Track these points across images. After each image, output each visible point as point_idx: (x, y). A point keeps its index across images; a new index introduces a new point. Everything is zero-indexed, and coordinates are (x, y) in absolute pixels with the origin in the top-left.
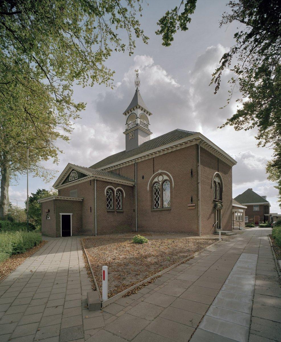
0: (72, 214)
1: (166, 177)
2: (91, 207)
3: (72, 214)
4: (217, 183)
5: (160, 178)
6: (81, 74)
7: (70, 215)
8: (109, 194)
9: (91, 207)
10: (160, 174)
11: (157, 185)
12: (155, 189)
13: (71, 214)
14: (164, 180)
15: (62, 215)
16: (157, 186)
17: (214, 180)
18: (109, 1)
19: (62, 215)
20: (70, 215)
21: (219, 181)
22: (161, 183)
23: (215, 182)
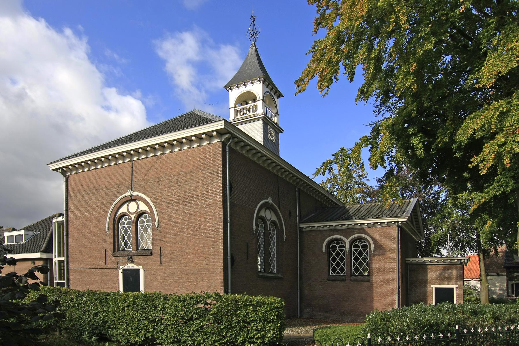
0: (457, 286)
1: (143, 207)
2: (106, 264)
3: (457, 286)
4: (268, 223)
5: (132, 207)
6: (462, 105)
7: (453, 289)
8: (360, 248)
9: (106, 264)
10: (132, 199)
11: (145, 218)
12: (142, 226)
13: (454, 287)
14: (139, 211)
15: (436, 289)
16: (126, 222)
17: (262, 214)
18: (323, 1)
19: (436, 289)
20: (453, 289)
21: (274, 218)
22: (133, 216)
23: (263, 219)
